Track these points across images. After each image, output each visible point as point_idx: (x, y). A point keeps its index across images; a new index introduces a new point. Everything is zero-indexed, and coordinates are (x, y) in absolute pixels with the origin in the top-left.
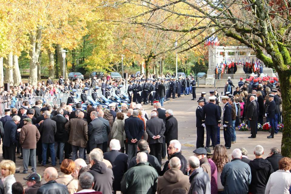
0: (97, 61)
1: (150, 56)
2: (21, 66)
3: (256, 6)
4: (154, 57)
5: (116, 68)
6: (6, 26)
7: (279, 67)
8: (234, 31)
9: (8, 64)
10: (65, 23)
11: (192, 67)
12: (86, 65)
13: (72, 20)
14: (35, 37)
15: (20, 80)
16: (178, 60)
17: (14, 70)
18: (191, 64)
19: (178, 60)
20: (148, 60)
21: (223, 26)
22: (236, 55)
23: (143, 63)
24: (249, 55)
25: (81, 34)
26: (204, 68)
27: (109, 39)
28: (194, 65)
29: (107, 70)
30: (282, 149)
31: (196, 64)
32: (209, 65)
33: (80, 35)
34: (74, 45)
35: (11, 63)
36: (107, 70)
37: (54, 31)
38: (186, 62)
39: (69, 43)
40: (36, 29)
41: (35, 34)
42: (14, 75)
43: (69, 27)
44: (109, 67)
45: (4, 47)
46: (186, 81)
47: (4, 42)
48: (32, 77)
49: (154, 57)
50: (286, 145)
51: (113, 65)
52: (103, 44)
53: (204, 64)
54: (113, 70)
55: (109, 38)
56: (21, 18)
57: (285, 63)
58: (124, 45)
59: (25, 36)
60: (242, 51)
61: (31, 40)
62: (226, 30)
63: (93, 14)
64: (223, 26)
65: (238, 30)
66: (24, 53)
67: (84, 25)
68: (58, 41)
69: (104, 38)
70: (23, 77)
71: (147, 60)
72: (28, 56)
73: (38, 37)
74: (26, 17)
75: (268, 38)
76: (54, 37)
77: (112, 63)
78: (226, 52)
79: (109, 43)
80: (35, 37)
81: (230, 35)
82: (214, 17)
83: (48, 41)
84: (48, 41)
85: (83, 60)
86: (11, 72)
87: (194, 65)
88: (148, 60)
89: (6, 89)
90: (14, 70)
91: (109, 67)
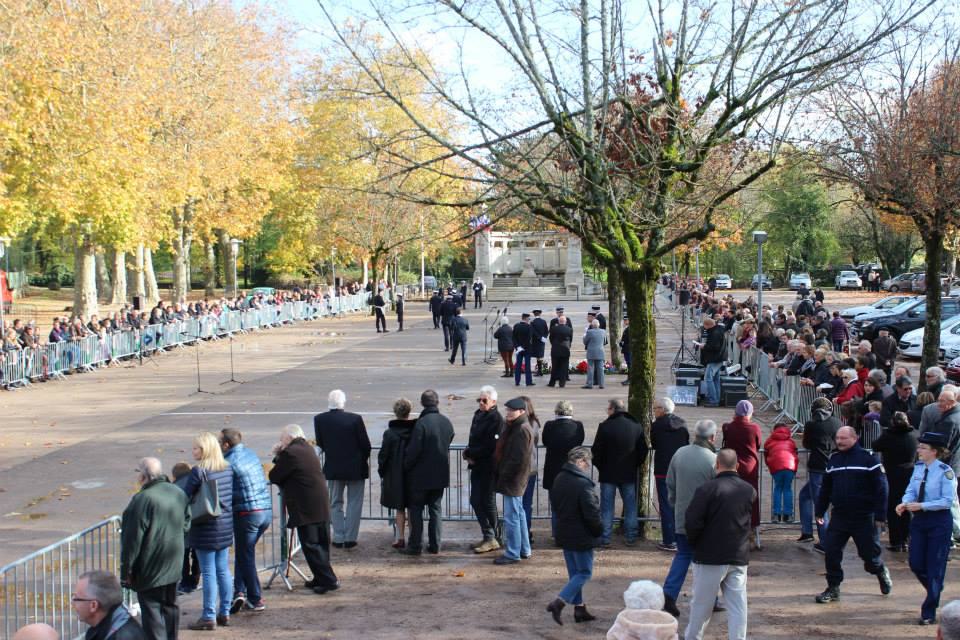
0: (288, 261)
1: (380, 249)
2: (156, 268)
3: (585, 162)
4: (386, 251)
5: (319, 270)
6: (132, 197)
7: (623, 265)
8: (546, 206)
9: (135, 264)
10: (233, 193)
11: (446, 267)
12: (268, 265)
13: (246, 188)
14: (181, 216)
15: (156, 292)
16: (424, 255)
17: (145, 273)
18: (445, 262)
19: (424, 255)
20: (377, 255)
21: (527, 198)
22: (522, 246)
23: (366, 261)
24: (544, 246)
25: (262, 212)
26: (466, 268)
27: (308, 220)
28: (450, 265)
29: (303, 273)
30: (630, 402)
31: (454, 262)
32: (477, 262)
33: (260, 215)
34: (249, 229)
35: (140, 262)
36: (303, 273)
37: (214, 206)
38: (437, 259)
39: (240, 228)
40: (183, 202)
41: (181, 212)
42: (146, 283)
43: (241, 199)
44: (308, 268)
45: (128, 234)
46: (701, 306)
47: (129, 226)
48: (177, 286)
49: (386, 251)
50: (636, 396)
51: (313, 264)
52: (298, 229)
53: (467, 262)
54: (314, 273)
55: (310, 222)
56: (155, 183)
57: (634, 258)
58: (335, 230)
59: (164, 215)
60: (530, 239)
61: (176, 220)
62: (534, 203)
63: (281, 177)
64: (527, 198)
65: (554, 203)
66: (163, 245)
67: (266, 196)
68: (222, 222)
69: (299, 219)
70: (161, 286)
71: (374, 255)
72: (171, 250)
73: (187, 217)
74: (164, 184)
75: (606, 216)
76: (214, 218)
77: (313, 261)
78: (505, 241)
79: (308, 227)
80: (181, 216)
81: (539, 211)
82: (514, 182)
83: (204, 223)
84: (204, 223)
85: (264, 256)
86: (141, 277)
87: (450, 265)
88: (377, 255)
89: (225, 335)
90: (145, 273)
91: (308, 268)
